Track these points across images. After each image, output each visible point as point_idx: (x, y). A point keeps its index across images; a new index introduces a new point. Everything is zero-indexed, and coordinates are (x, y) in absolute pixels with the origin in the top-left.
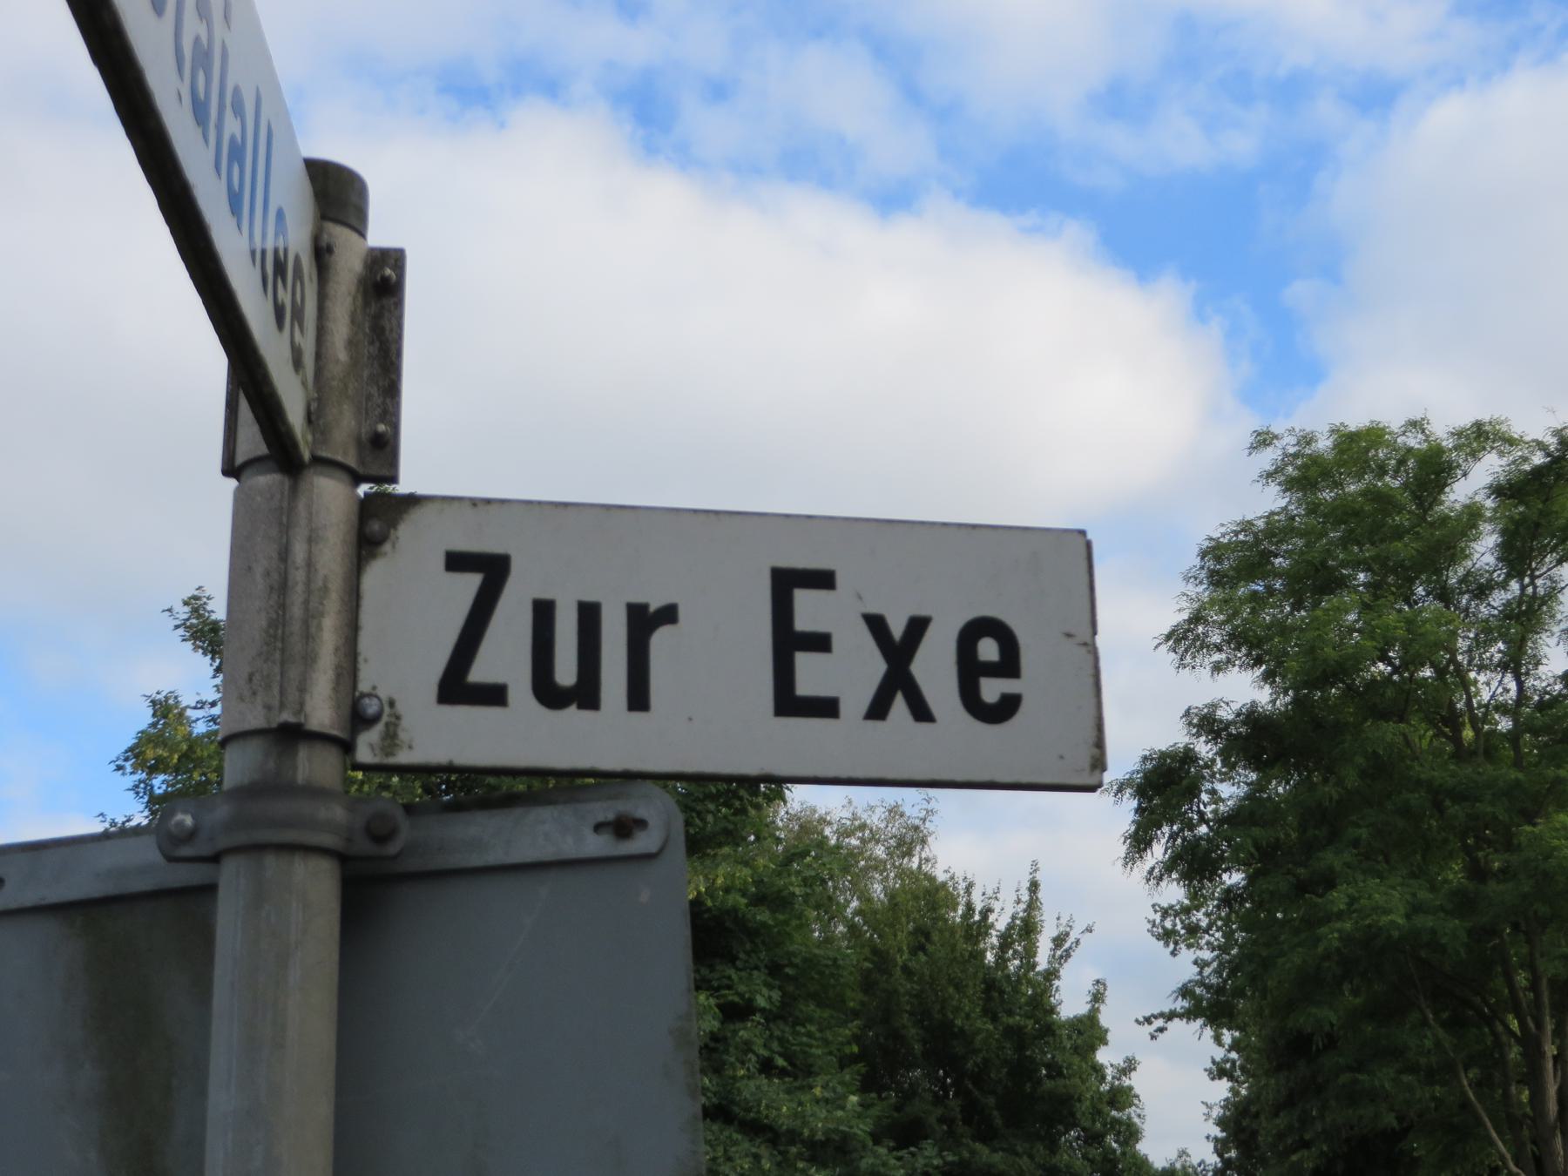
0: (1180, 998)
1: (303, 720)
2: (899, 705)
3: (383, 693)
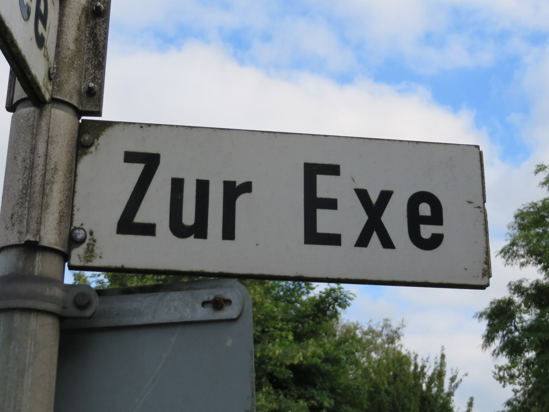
0: (507, 406)
1: (38, 240)
2: (375, 239)
3: (87, 228)
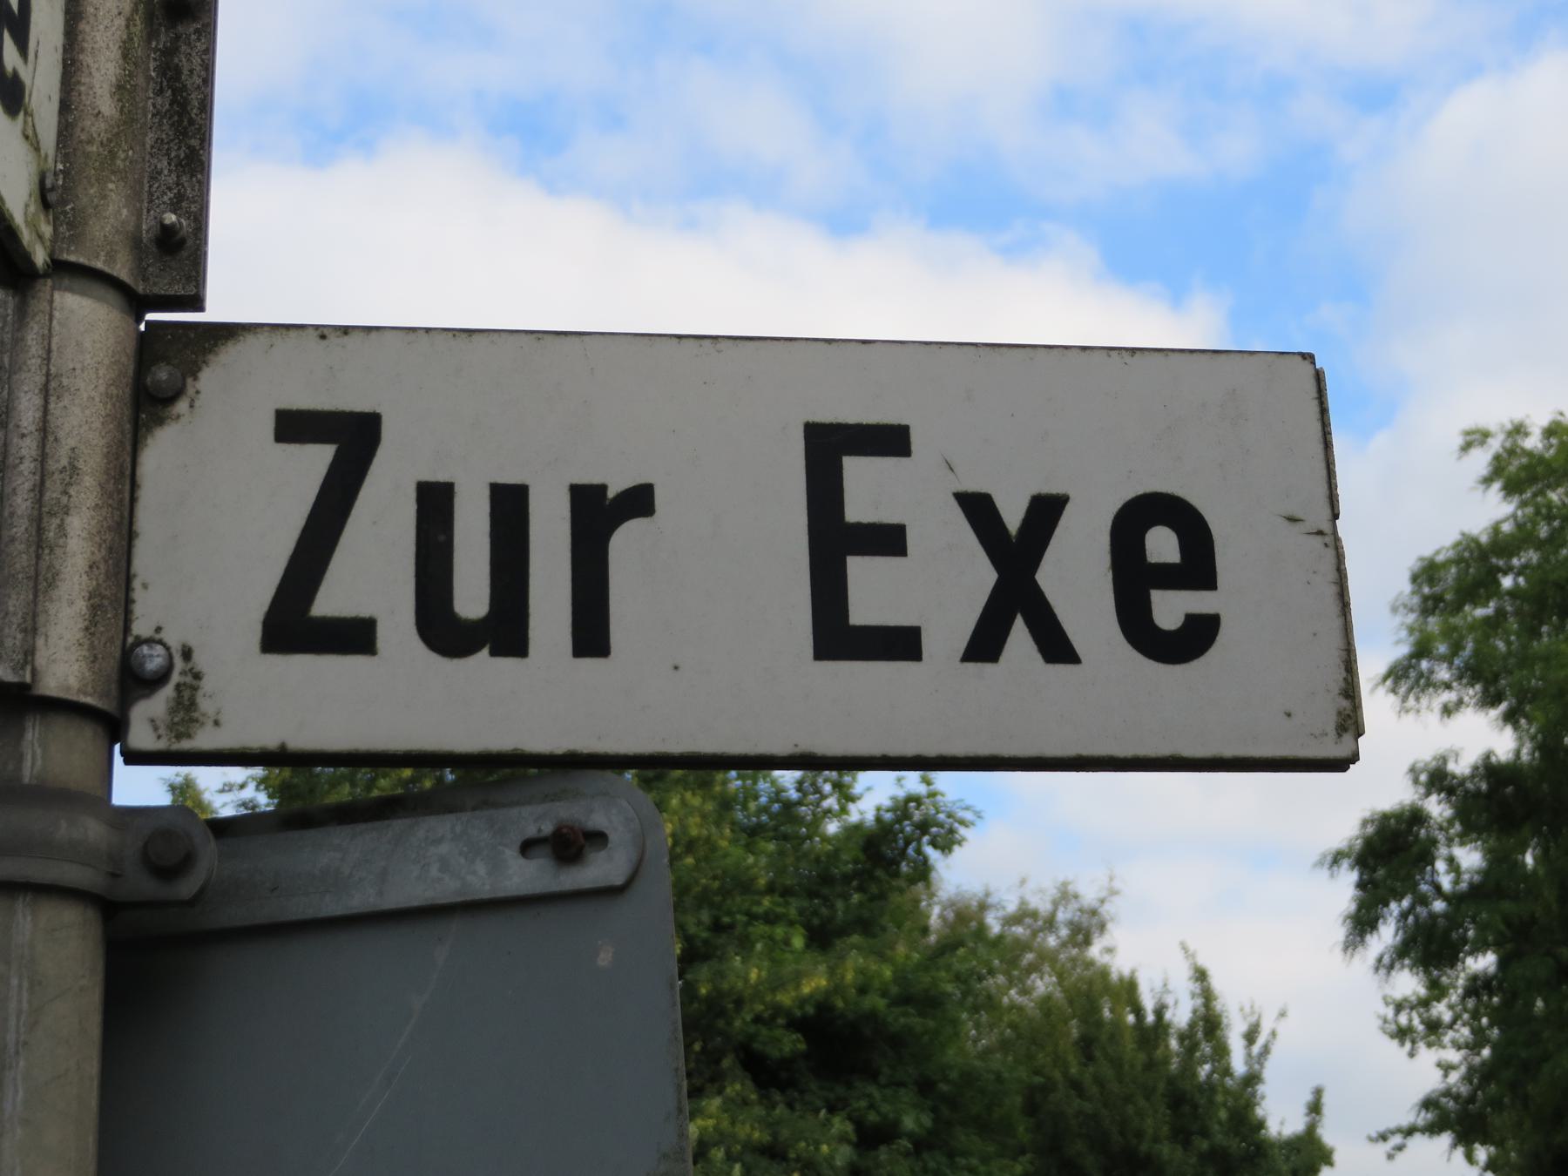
1: (28, 679)
2: (1020, 637)
3: (173, 638)
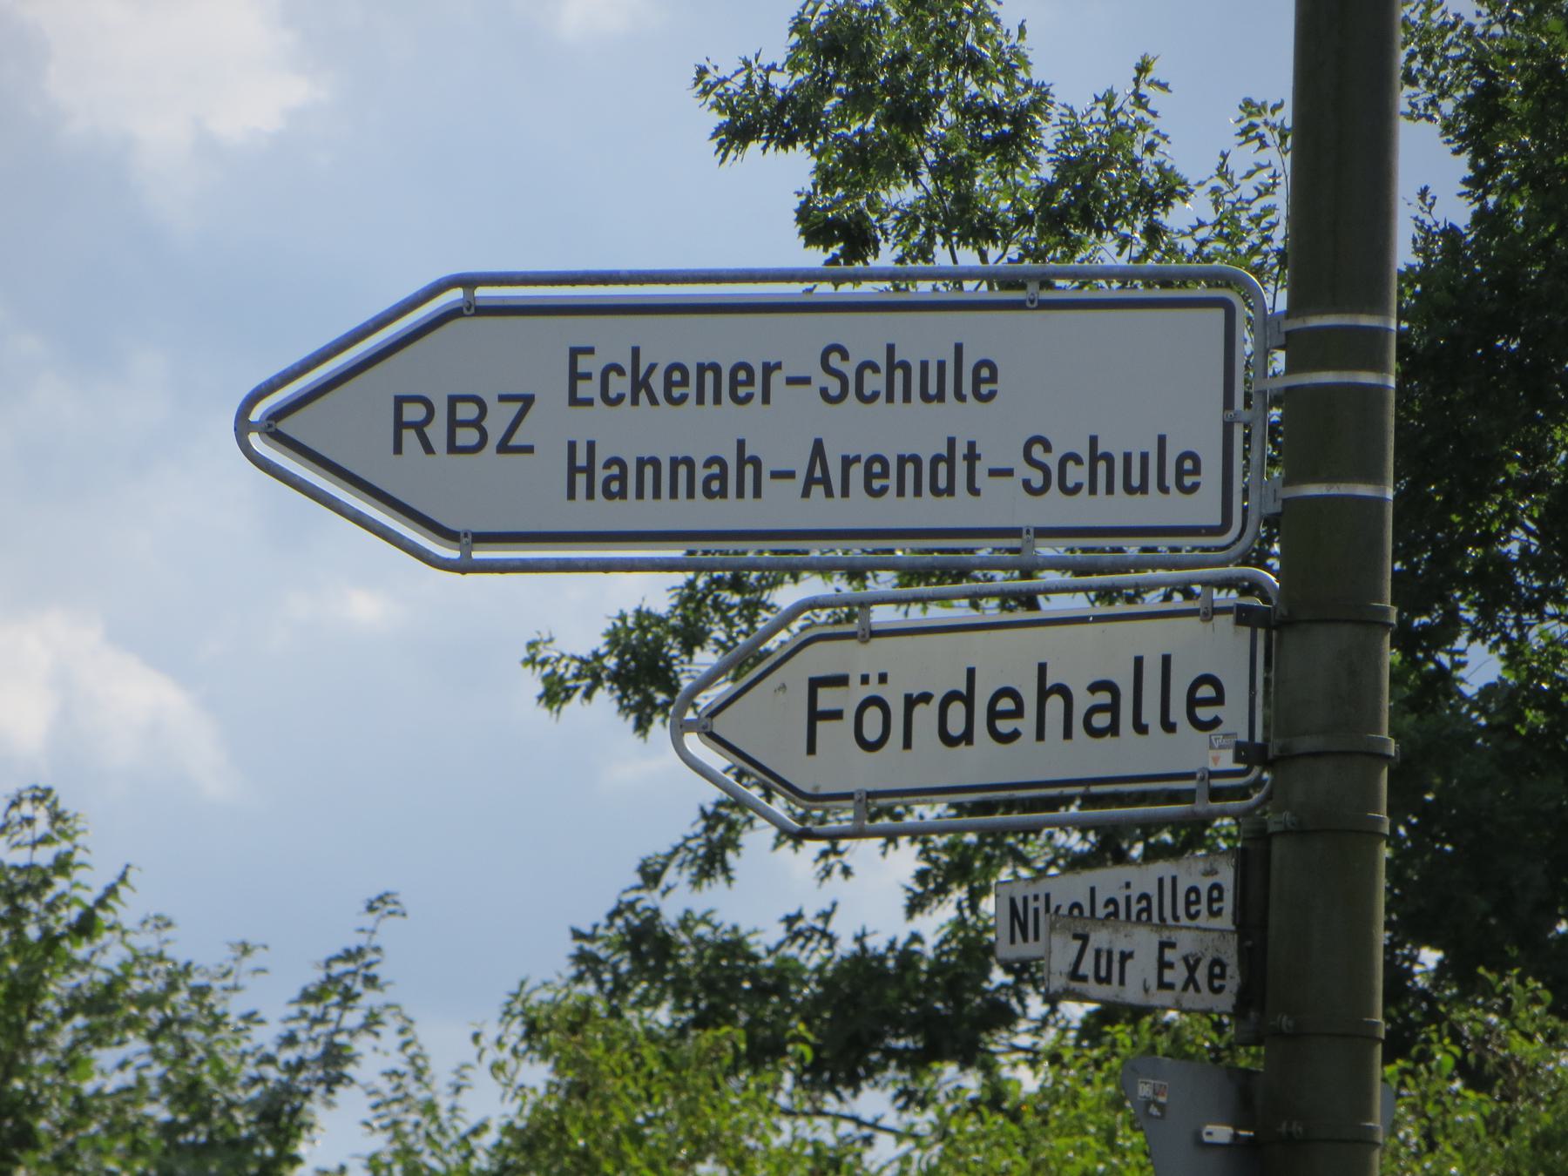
2: (1191, 987)
